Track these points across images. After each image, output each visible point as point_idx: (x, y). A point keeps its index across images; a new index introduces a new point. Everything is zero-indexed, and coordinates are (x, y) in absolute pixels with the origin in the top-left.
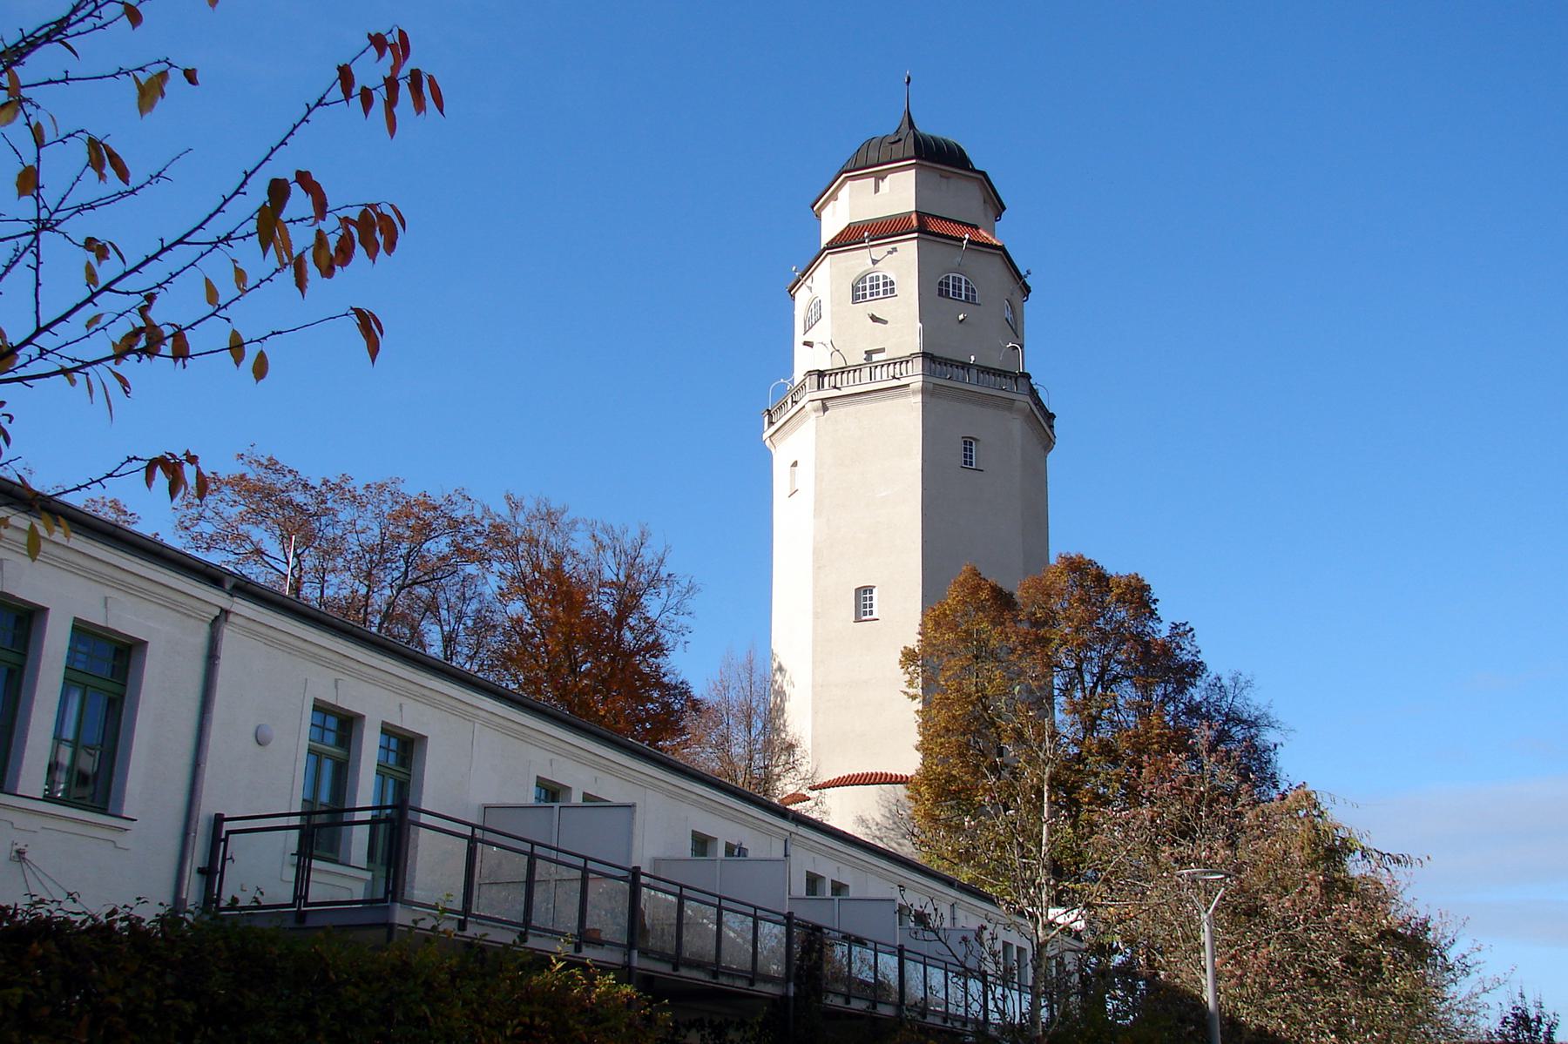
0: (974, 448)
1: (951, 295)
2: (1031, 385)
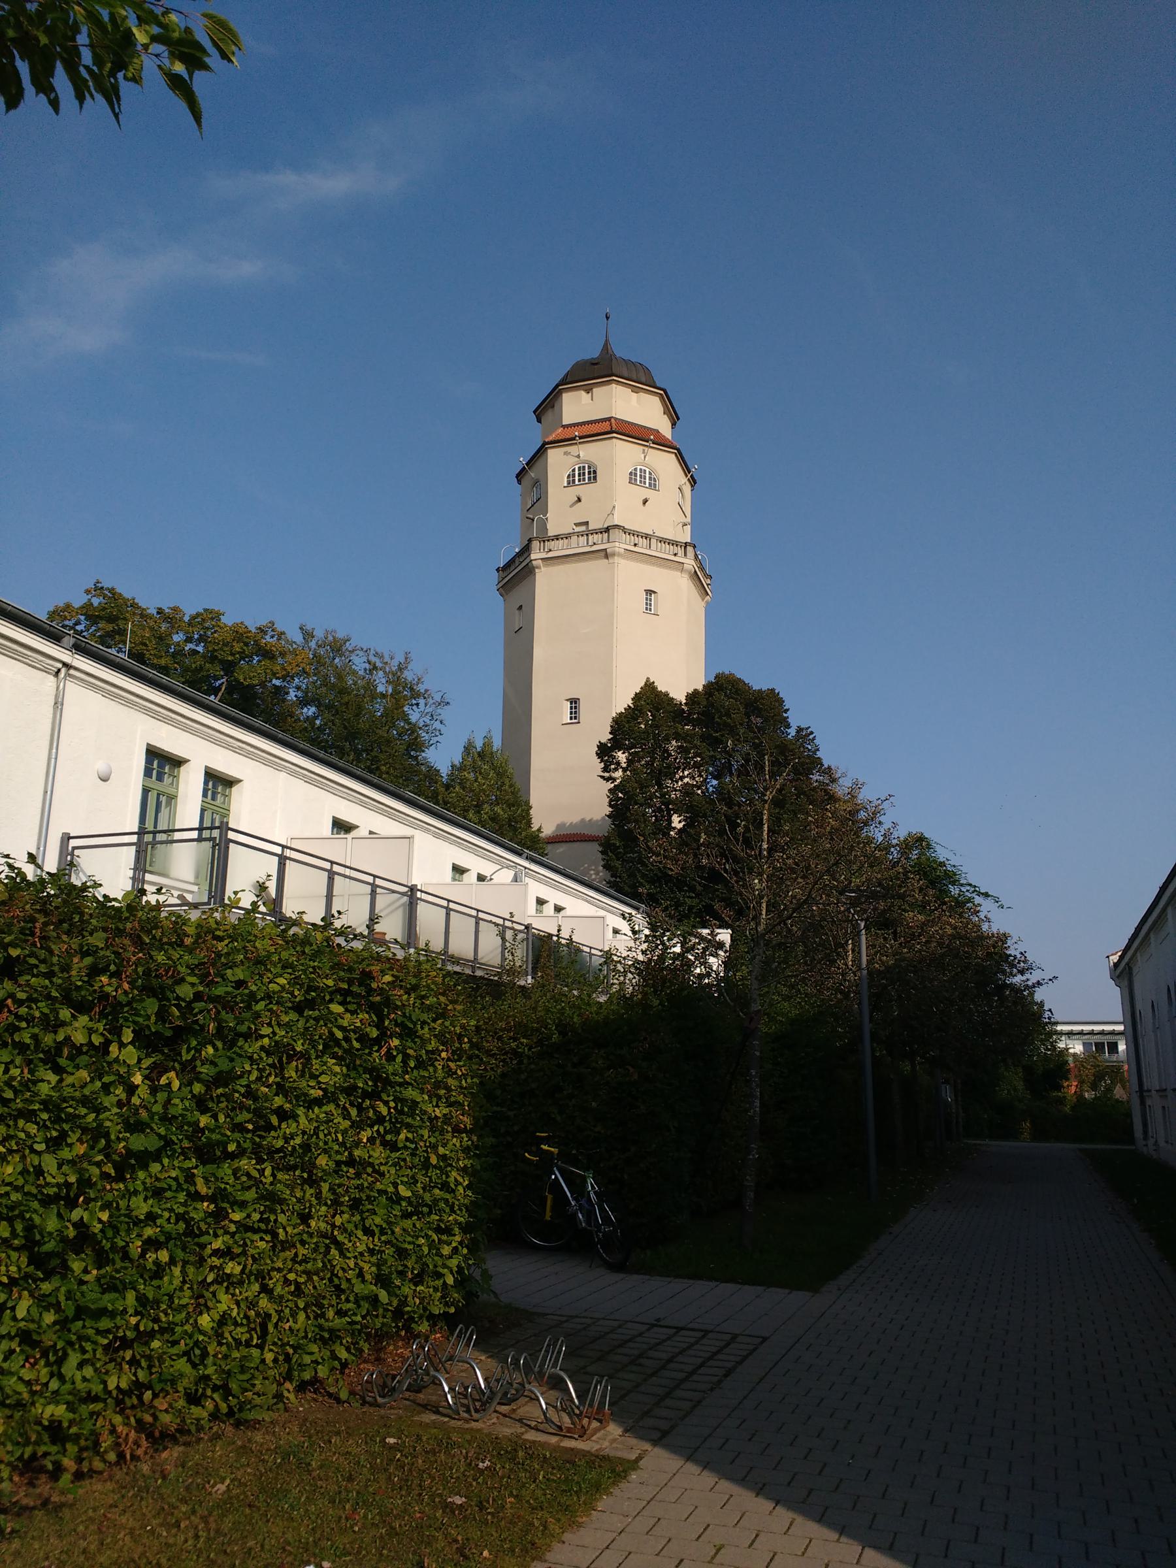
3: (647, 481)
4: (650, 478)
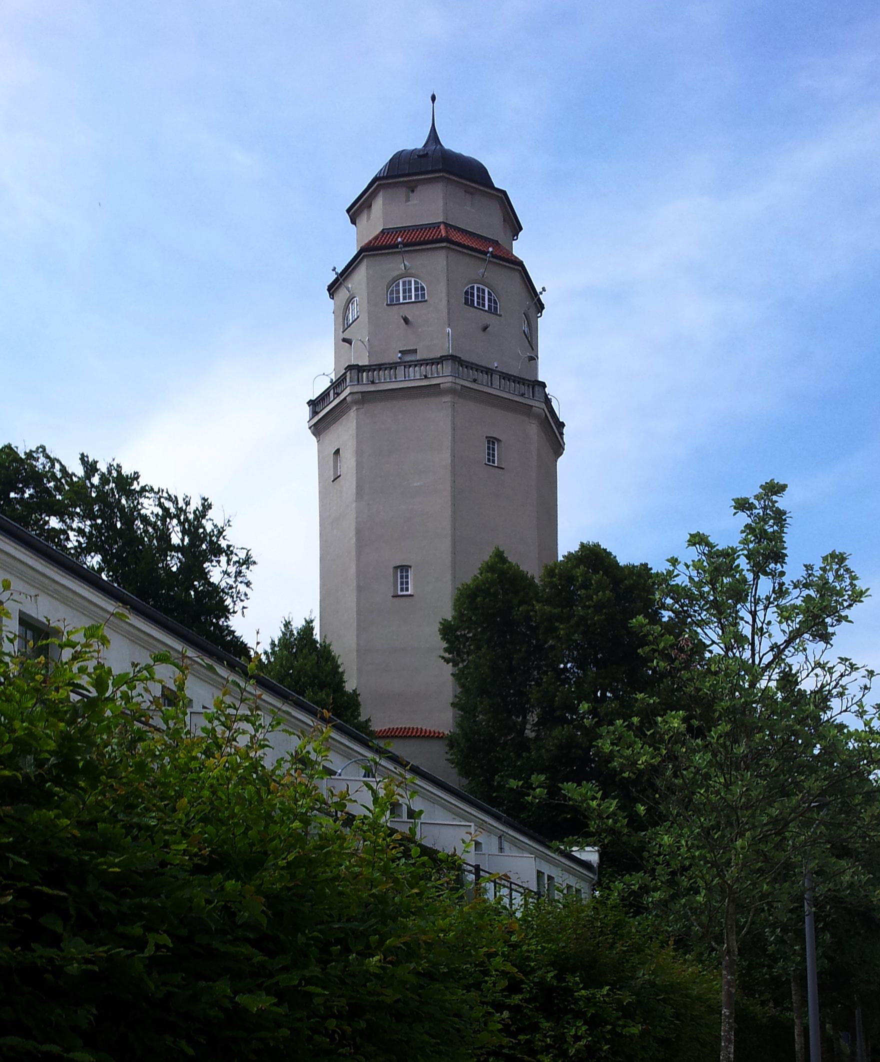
2: (546, 395)
4: (416, 289)
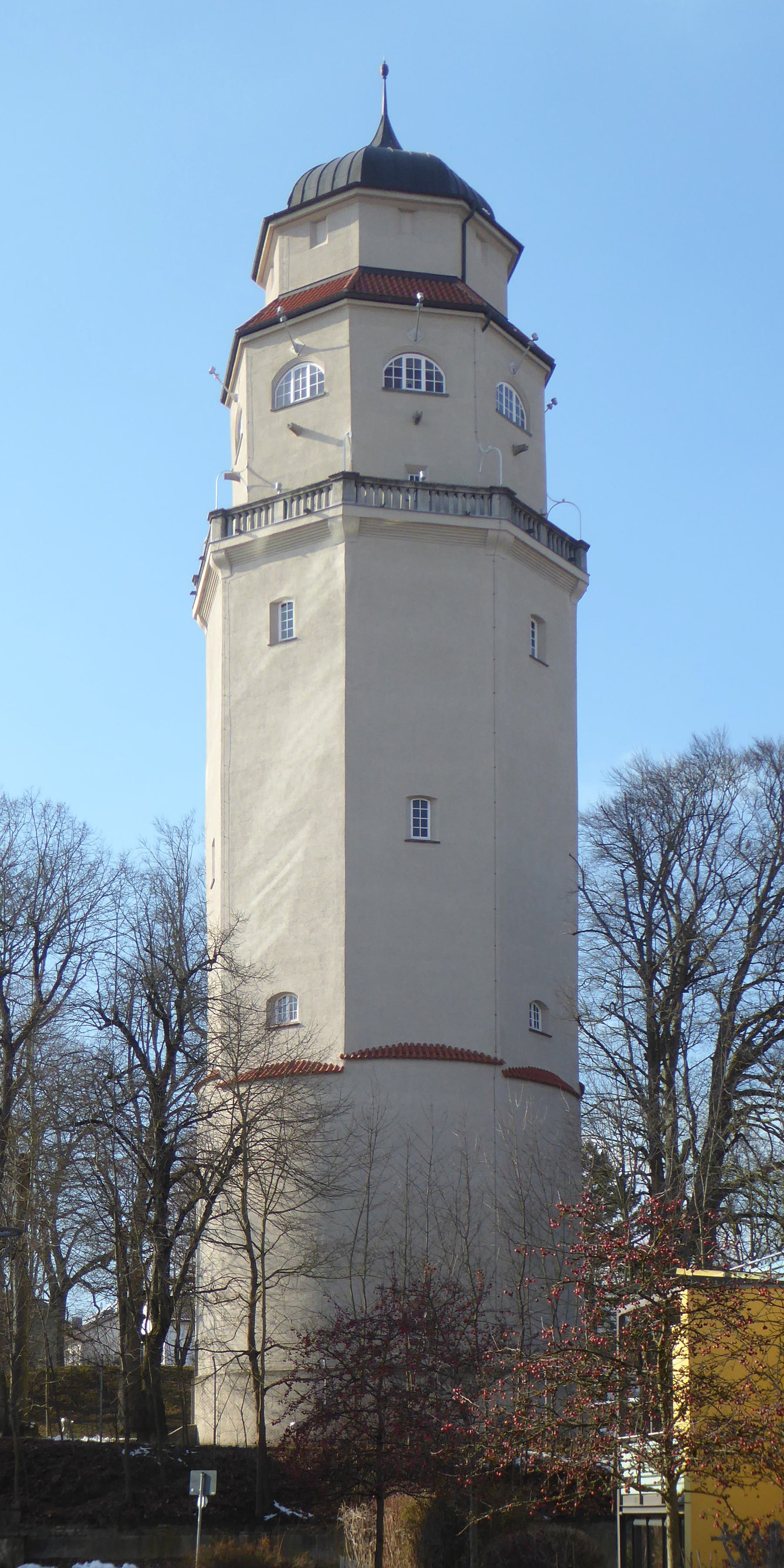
0: (429, 809)
1: (404, 386)
3: (423, 380)
4: (429, 376)
